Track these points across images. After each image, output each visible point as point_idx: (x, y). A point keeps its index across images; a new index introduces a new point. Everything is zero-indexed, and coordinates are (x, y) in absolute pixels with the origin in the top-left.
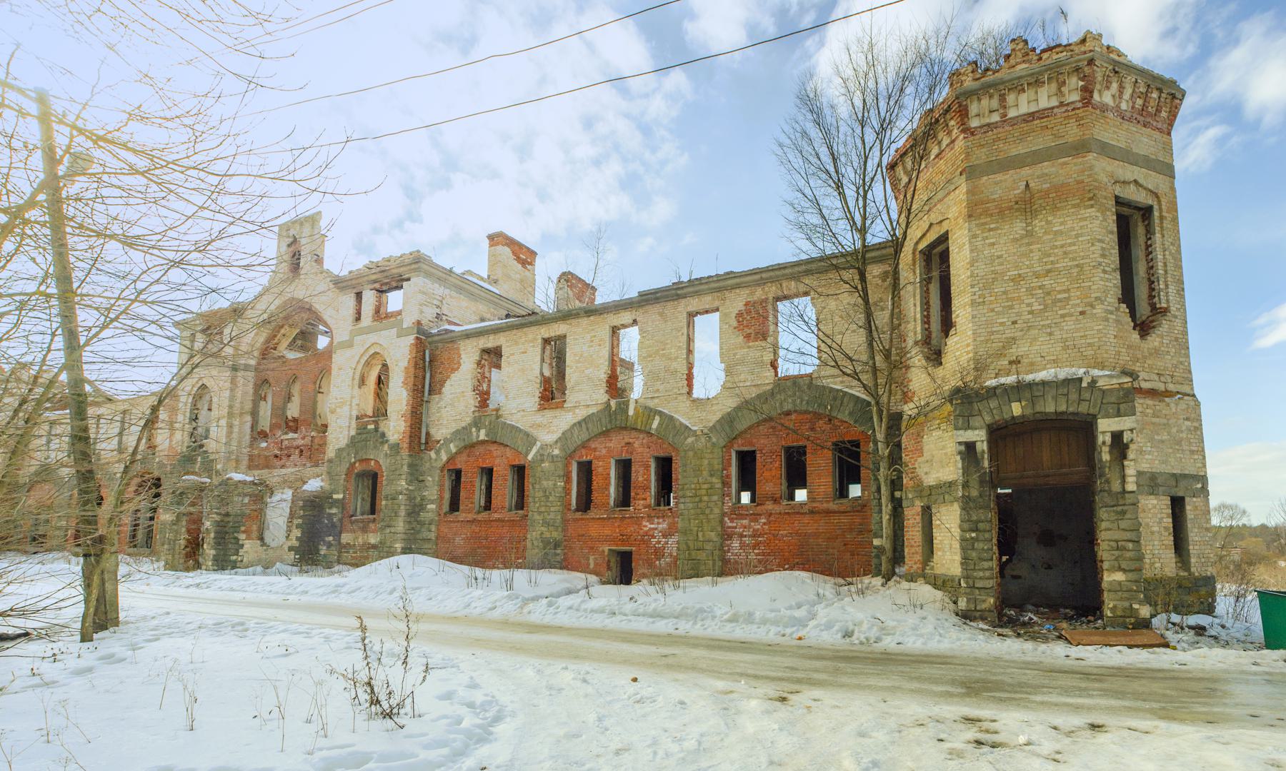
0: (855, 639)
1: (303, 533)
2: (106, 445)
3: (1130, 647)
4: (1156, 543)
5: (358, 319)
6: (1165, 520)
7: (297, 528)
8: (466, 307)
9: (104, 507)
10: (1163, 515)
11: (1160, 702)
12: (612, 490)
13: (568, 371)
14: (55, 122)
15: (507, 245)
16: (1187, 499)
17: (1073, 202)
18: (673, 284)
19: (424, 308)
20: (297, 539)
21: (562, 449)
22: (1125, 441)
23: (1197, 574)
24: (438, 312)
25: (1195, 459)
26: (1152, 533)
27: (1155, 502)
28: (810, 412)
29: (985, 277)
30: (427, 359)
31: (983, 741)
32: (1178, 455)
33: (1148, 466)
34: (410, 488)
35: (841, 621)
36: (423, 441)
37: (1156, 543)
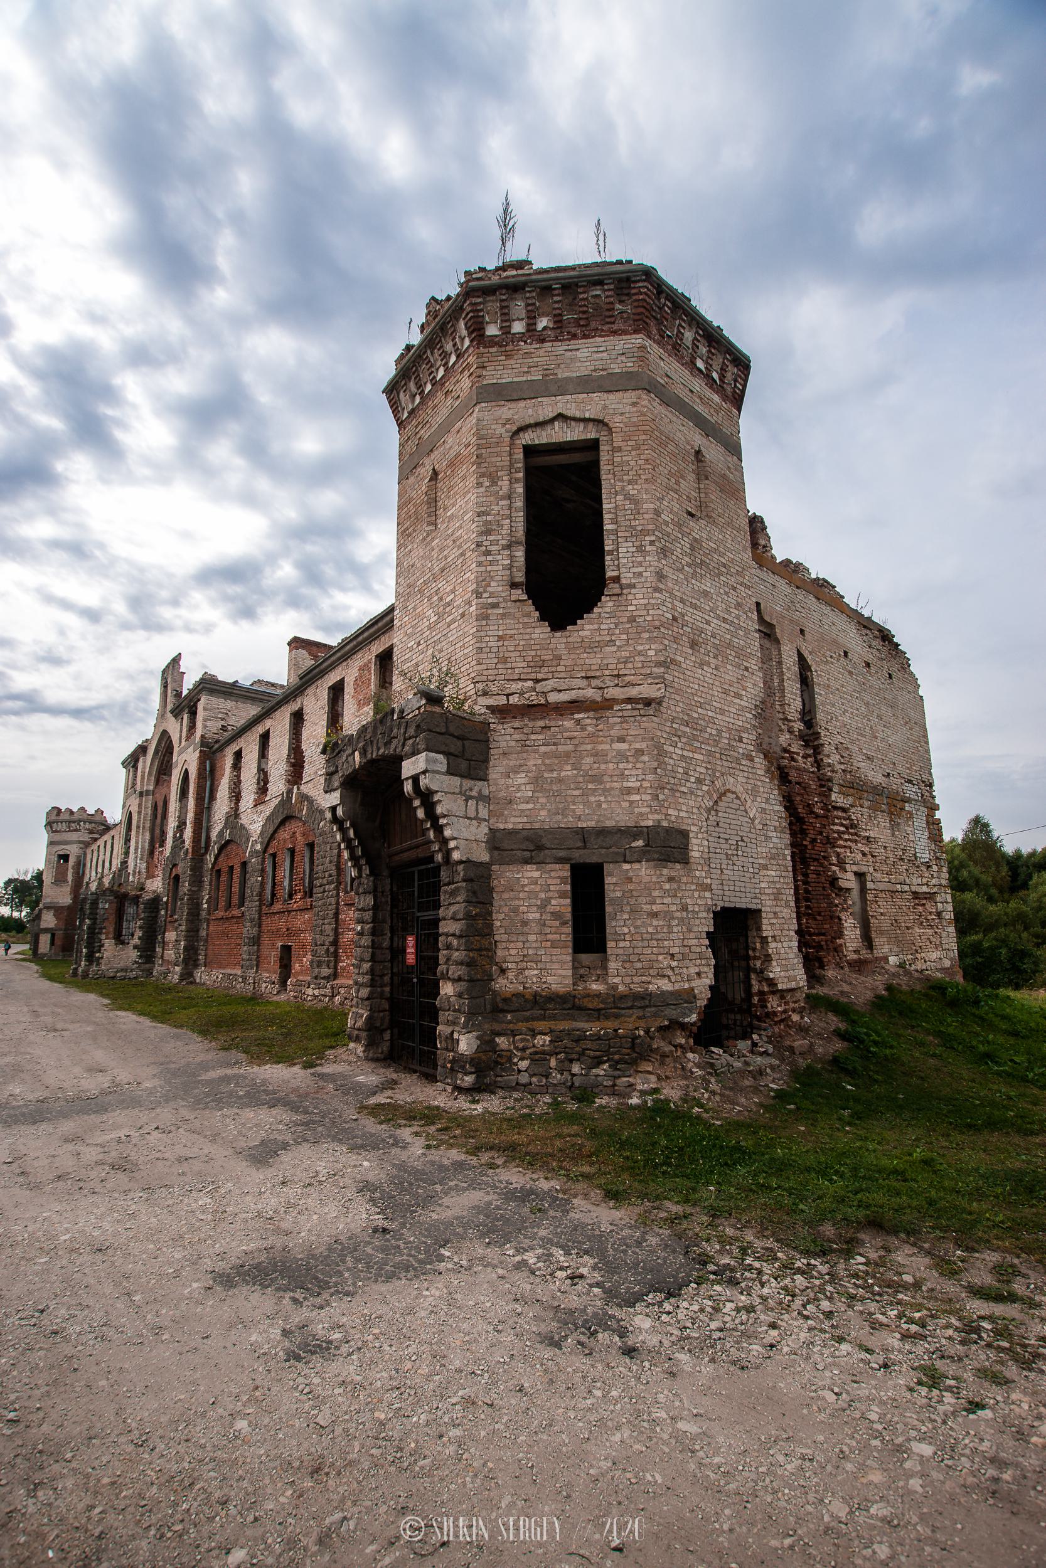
0: (869, 657)
1: (143, 935)
2: (551, 326)
3: (822, 590)
4: (532, 938)
5: (287, 950)
6: (553, 902)
7: (134, 948)
8: (578, 1268)
9: (1017, 1317)
10: (551, 894)
11: (139, 813)
12: (373, 687)
13: (778, 841)
14: (205, 1067)
15: (303, 647)
16: (608, 868)
17: (468, 516)
18: (682, 294)
19: (208, 723)
20: (140, 938)
21: (261, 843)
22: (600, 699)
23: (621, 988)
24: (223, 723)
25: (631, 803)
26: (525, 923)
27: (537, 874)
28: (214, 1548)
29: (485, 673)
30: (208, 769)
31: (43, 666)
32: (592, 799)
33: (525, 820)
34: (193, 889)
35: (974, 1014)
36: (203, 845)
37: (532, 938)
